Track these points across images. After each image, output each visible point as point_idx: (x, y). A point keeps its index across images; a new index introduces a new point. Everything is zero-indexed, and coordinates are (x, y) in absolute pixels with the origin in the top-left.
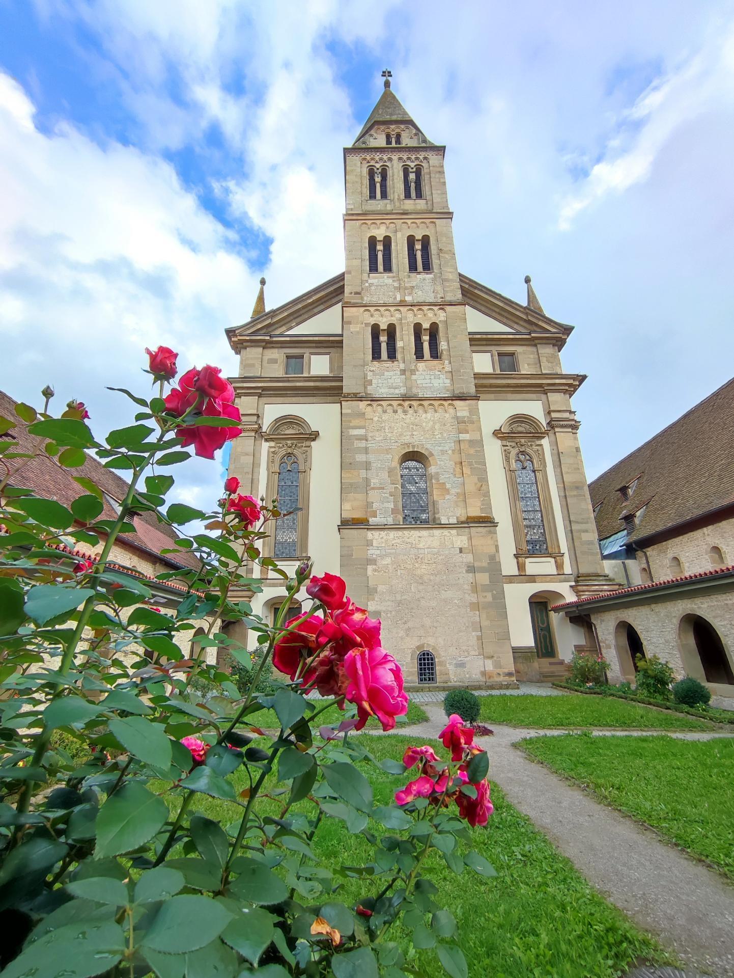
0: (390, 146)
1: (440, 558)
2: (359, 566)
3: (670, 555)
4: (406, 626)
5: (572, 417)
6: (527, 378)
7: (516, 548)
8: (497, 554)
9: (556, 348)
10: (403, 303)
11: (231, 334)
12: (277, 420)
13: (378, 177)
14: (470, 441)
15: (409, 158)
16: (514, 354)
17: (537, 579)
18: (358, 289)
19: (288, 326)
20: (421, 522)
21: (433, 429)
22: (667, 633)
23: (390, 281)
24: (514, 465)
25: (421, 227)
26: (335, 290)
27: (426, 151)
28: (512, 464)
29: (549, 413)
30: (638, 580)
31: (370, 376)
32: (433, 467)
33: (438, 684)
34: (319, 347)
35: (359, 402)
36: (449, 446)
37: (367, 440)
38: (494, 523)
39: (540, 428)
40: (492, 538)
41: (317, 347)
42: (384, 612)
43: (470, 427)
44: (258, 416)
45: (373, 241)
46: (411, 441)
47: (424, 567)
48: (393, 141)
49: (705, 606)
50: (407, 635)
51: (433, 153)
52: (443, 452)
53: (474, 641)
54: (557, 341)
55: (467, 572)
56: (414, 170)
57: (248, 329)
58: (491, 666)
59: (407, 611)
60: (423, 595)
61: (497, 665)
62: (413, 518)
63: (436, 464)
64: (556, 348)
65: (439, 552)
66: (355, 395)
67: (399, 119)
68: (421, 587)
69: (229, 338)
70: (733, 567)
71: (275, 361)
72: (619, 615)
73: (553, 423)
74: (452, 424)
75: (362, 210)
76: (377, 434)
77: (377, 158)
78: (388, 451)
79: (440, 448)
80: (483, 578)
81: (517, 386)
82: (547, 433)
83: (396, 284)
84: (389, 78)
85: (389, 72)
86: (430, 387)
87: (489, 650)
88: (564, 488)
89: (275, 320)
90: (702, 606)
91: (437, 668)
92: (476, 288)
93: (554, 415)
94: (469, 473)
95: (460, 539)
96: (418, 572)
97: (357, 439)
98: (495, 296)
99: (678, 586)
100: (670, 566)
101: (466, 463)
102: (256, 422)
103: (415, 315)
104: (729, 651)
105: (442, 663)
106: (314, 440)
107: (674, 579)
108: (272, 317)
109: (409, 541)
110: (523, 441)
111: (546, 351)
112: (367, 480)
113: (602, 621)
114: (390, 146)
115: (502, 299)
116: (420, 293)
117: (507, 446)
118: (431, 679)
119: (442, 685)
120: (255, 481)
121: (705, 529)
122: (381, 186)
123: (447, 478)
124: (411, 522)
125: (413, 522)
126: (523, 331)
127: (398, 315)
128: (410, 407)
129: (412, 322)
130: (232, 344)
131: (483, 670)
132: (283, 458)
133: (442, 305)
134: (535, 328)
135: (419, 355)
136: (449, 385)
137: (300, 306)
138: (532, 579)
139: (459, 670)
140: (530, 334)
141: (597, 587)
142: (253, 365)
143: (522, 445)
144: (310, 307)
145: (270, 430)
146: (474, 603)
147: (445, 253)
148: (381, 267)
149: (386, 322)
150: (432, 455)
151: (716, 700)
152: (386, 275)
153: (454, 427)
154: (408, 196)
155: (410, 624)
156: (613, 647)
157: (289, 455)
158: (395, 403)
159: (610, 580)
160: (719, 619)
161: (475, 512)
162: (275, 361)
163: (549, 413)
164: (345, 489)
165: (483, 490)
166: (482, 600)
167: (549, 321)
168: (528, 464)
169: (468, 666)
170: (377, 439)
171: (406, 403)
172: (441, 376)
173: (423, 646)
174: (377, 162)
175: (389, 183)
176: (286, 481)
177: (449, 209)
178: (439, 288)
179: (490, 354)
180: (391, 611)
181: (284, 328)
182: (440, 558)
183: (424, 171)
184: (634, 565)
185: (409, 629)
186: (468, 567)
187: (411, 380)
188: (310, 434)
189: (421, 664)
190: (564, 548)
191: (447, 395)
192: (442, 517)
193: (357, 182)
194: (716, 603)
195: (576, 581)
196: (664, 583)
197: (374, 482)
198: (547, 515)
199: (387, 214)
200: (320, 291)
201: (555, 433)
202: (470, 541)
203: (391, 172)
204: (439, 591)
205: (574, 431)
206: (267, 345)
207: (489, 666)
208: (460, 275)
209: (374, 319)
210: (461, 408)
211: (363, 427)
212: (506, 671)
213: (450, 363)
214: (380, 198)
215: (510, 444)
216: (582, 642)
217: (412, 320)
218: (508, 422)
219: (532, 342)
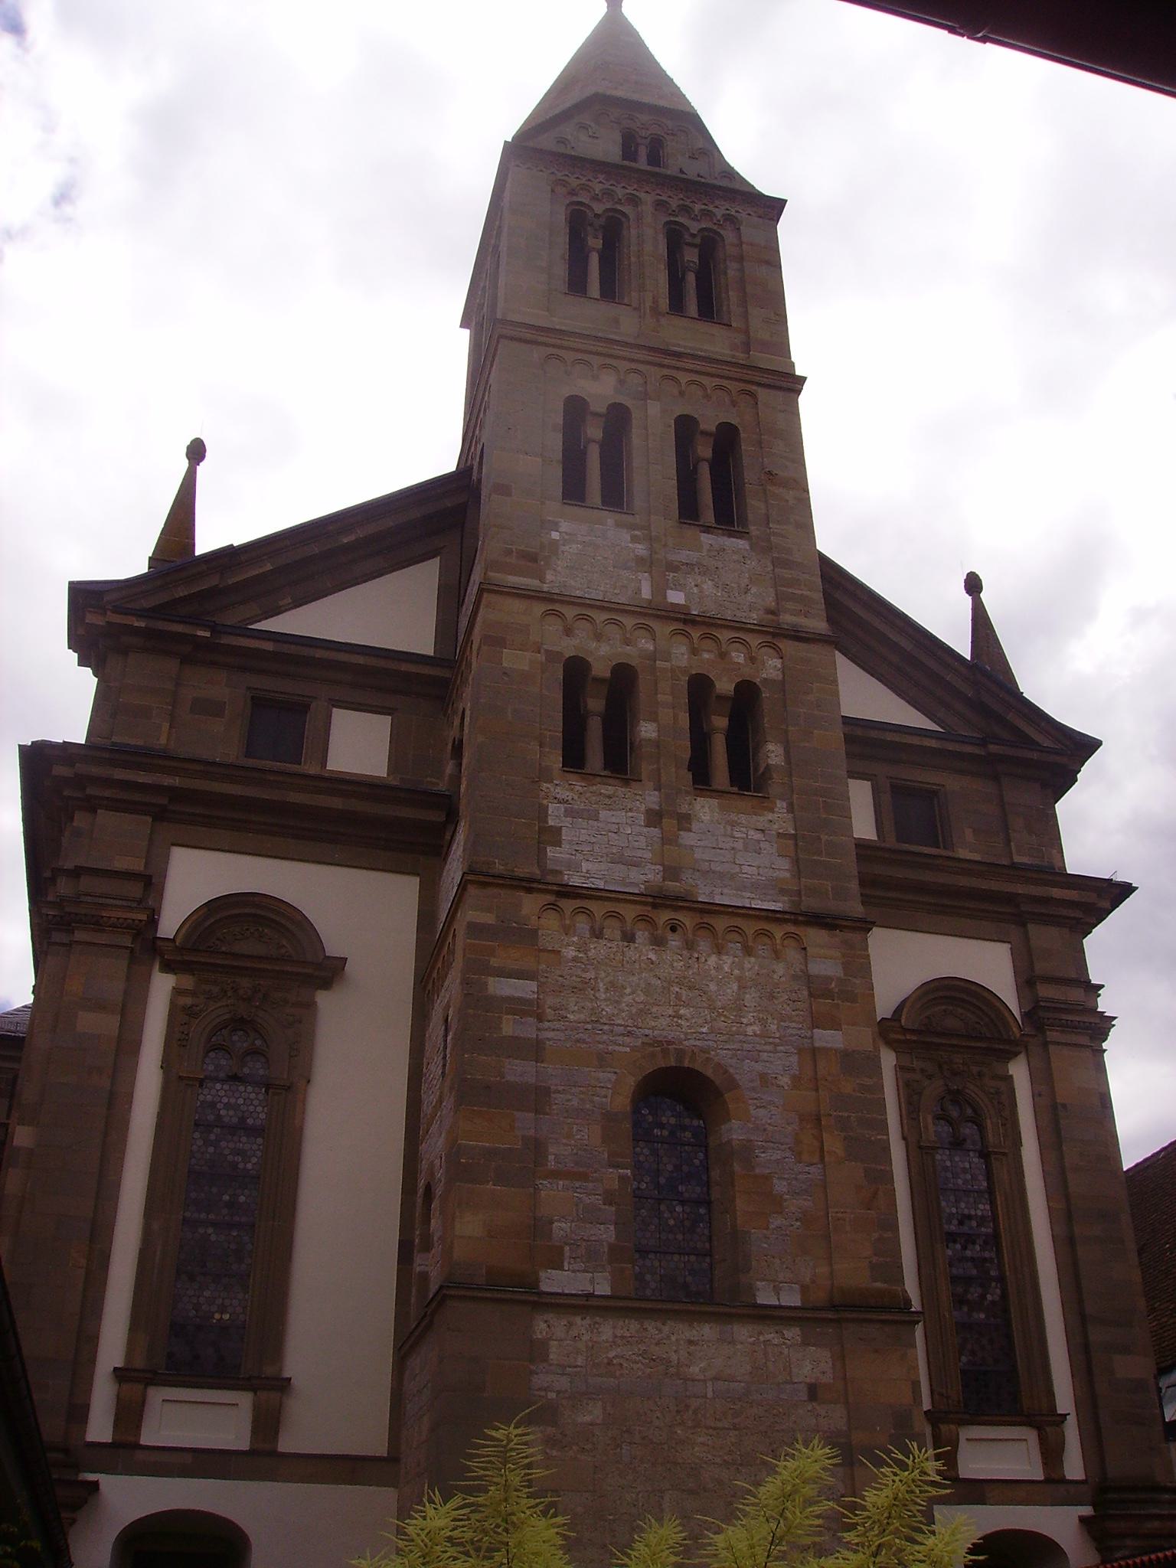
0: (633, 164)
12: (213, 907)
16: (935, 793)
28: (926, 1127)
31: (555, 815)
32: (735, 1123)
36: (782, 1065)
37: (540, 1018)
45: (575, 410)
47: (700, 1440)
48: (643, 152)
52: (765, 1079)
56: (698, 241)
71: (211, 708)
74: (794, 996)
77: (598, 188)
78: (603, 1060)
79: (758, 1067)
88: (1064, 1213)
93: (1045, 991)
99: (645, 1310)
102: (140, 902)
103: (694, 652)
106: (326, 984)
112: (537, 1147)
114: (633, 164)
123: (777, 1162)
128: (673, 929)
130: (81, 631)
136: (788, 875)
150: (733, 1084)
158: (629, 912)
162: (211, 708)
170: (571, 1017)
171: (664, 917)
172: (762, 845)
174: (595, 198)
190: (1064, 1399)
197: (558, 1153)
201: (1045, 1045)
209: (575, 642)
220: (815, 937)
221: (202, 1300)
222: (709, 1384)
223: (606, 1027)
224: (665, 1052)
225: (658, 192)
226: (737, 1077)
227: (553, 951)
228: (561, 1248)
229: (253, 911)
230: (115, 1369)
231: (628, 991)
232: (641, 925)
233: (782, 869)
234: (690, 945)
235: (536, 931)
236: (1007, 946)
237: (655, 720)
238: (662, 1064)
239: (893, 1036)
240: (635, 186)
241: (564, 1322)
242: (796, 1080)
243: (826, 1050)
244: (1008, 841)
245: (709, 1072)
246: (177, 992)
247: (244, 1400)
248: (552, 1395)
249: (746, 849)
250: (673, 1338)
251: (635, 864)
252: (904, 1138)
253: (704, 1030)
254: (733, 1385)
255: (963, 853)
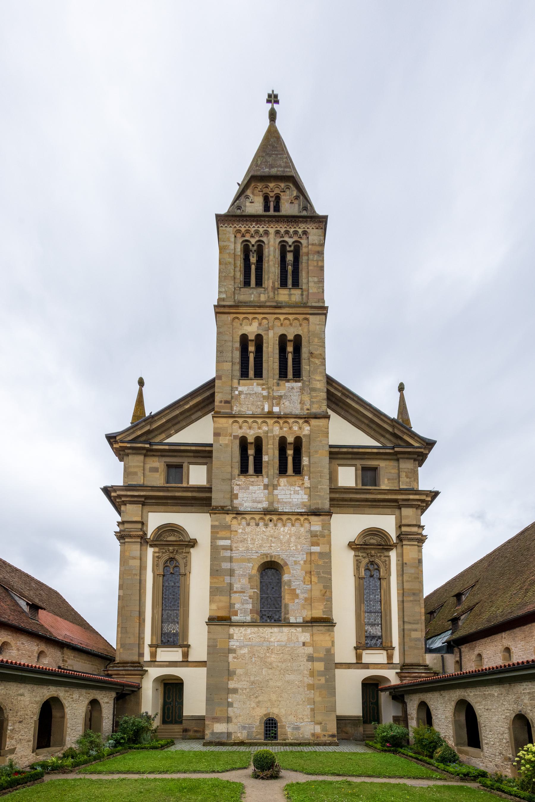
1: (287, 649)
2: (222, 654)
3: (476, 652)
4: (257, 700)
5: (420, 531)
6: (385, 494)
7: (357, 642)
8: (332, 648)
9: (417, 463)
10: (270, 415)
11: (112, 440)
12: (159, 528)
13: (253, 257)
14: (320, 553)
15: (287, 232)
16: (377, 468)
17: (370, 666)
18: (228, 398)
19: (167, 433)
20: (275, 621)
21: (289, 542)
22: (447, 711)
23: (259, 389)
24: (363, 573)
25: (293, 325)
26: (204, 400)
27: (306, 222)
29: (400, 527)
30: (451, 670)
33: (278, 741)
34: (197, 457)
35: (226, 515)
36: (301, 558)
37: (231, 550)
38: (333, 623)
39: (389, 541)
40: (329, 635)
41: (194, 457)
42: (241, 689)
43: (322, 540)
44: (143, 523)
45: (244, 339)
46: (269, 552)
49: (472, 694)
50: (258, 706)
51: (314, 225)
52: (296, 562)
53: (308, 712)
54: (418, 456)
55: (308, 660)
56: (292, 248)
57: (129, 435)
58: (319, 730)
59: (258, 689)
60: (271, 677)
61: (324, 729)
62: (268, 617)
63: (289, 573)
64: (417, 463)
65: (286, 645)
66: (223, 508)
67: (279, 174)
68: (270, 671)
69: (111, 444)
70: (533, 661)
72: (421, 697)
73: (401, 536)
74: (306, 537)
75: (235, 301)
76: (240, 545)
78: (249, 560)
79: (294, 559)
80: (320, 666)
81: (375, 500)
82: (395, 546)
83: (265, 393)
84: (275, 106)
85: (276, 96)
86: (290, 503)
87: (319, 718)
89: (154, 426)
90: (471, 694)
91: (279, 730)
92: (348, 397)
93: (404, 529)
94: (317, 581)
95: (303, 636)
96: (269, 660)
97: (224, 549)
98: (365, 406)
100: (475, 661)
101: (315, 573)
102: (141, 529)
104: (480, 727)
105: (283, 727)
106: (193, 546)
107: (477, 670)
108: (151, 423)
109: (262, 635)
110: (373, 552)
111: (406, 465)
112: (231, 585)
113: (411, 700)
115: (372, 410)
116: (287, 403)
117: (359, 556)
118: (275, 738)
119: (281, 741)
120: (143, 582)
121: (503, 634)
122: (256, 269)
123: (298, 585)
124: (266, 620)
125: (268, 621)
126: (389, 445)
127: (265, 428)
128: (271, 521)
129: (277, 436)
130: (115, 450)
131: (313, 732)
132: (166, 562)
133: (307, 418)
134: (402, 444)
135: (283, 470)
136: (307, 500)
137: (177, 412)
138: (367, 666)
139: (295, 732)
140: (393, 448)
141: (416, 674)
142: (135, 473)
143: (372, 556)
144: (188, 414)
145: (154, 537)
146: (311, 685)
147: (315, 357)
148: (251, 373)
149: (254, 434)
150: (286, 564)
151: (468, 759)
152: (255, 382)
153: (308, 540)
154: (284, 284)
155: (260, 698)
156: (415, 719)
157: (172, 559)
158: (257, 517)
159: (429, 669)
160: (478, 704)
161: (318, 613)
162: (155, 470)
163: (400, 527)
164: (214, 591)
165: (327, 596)
166: (317, 682)
167: (414, 435)
168: (376, 574)
169: (302, 729)
170: (240, 549)
171: (268, 517)
172: (300, 492)
173: (269, 714)
174: (252, 236)
175: (265, 265)
176: (170, 582)
177: (324, 302)
178: (306, 398)
179: (354, 468)
180: (246, 689)
181: (163, 436)
182: (287, 649)
183: (304, 250)
184: (450, 659)
185: (259, 702)
186: (309, 657)
187: (273, 495)
188: (189, 542)
189: (266, 727)
190: (396, 641)
191: (303, 510)
192: (291, 617)
193: (230, 263)
194: (478, 693)
195: (401, 669)
196: (469, 672)
197: (237, 586)
198: (386, 616)
199: (260, 307)
200: (197, 396)
201: (402, 546)
202: (312, 637)
203: (267, 250)
204: (284, 675)
205: (420, 544)
206: (148, 453)
207: (318, 729)
208: (330, 381)
209: (242, 431)
210: (315, 523)
211: (229, 538)
212: (330, 733)
213: (309, 479)
214: (254, 286)
215: (362, 554)
216: (400, 714)
217: (277, 433)
218: (362, 534)
219: (396, 457)
220: (313, 518)
221: (169, 628)
222: (276, 643)
223: (250, 551)
224: (267, 557)
225: (276, 226)
226: (287, 562)
227: (235, 531)
228: (237, 611)
229: (171, 528)
230: (354, 647)
231: (257, 540)
232: (261, 521)
233: (305, 498)
234: (275, 525)
235: (230, 526)
236: (394, 516)
237: (268, 455)
238: (266, 560)
239: (353, 547)
240: (267, 225)
241: (238, 629)
242: (305, 562)
243: (314, 553)
244: (399, 481)
245: (279, 561)
246: (154, 552)
247: (180, 650)
248: (234, 647)
249: (294, 493)
250: (267, 632)
251: (259, 502)
252: (355, 576)
253: (279, 550)
254: (282, 643)
255: (383, 487)
